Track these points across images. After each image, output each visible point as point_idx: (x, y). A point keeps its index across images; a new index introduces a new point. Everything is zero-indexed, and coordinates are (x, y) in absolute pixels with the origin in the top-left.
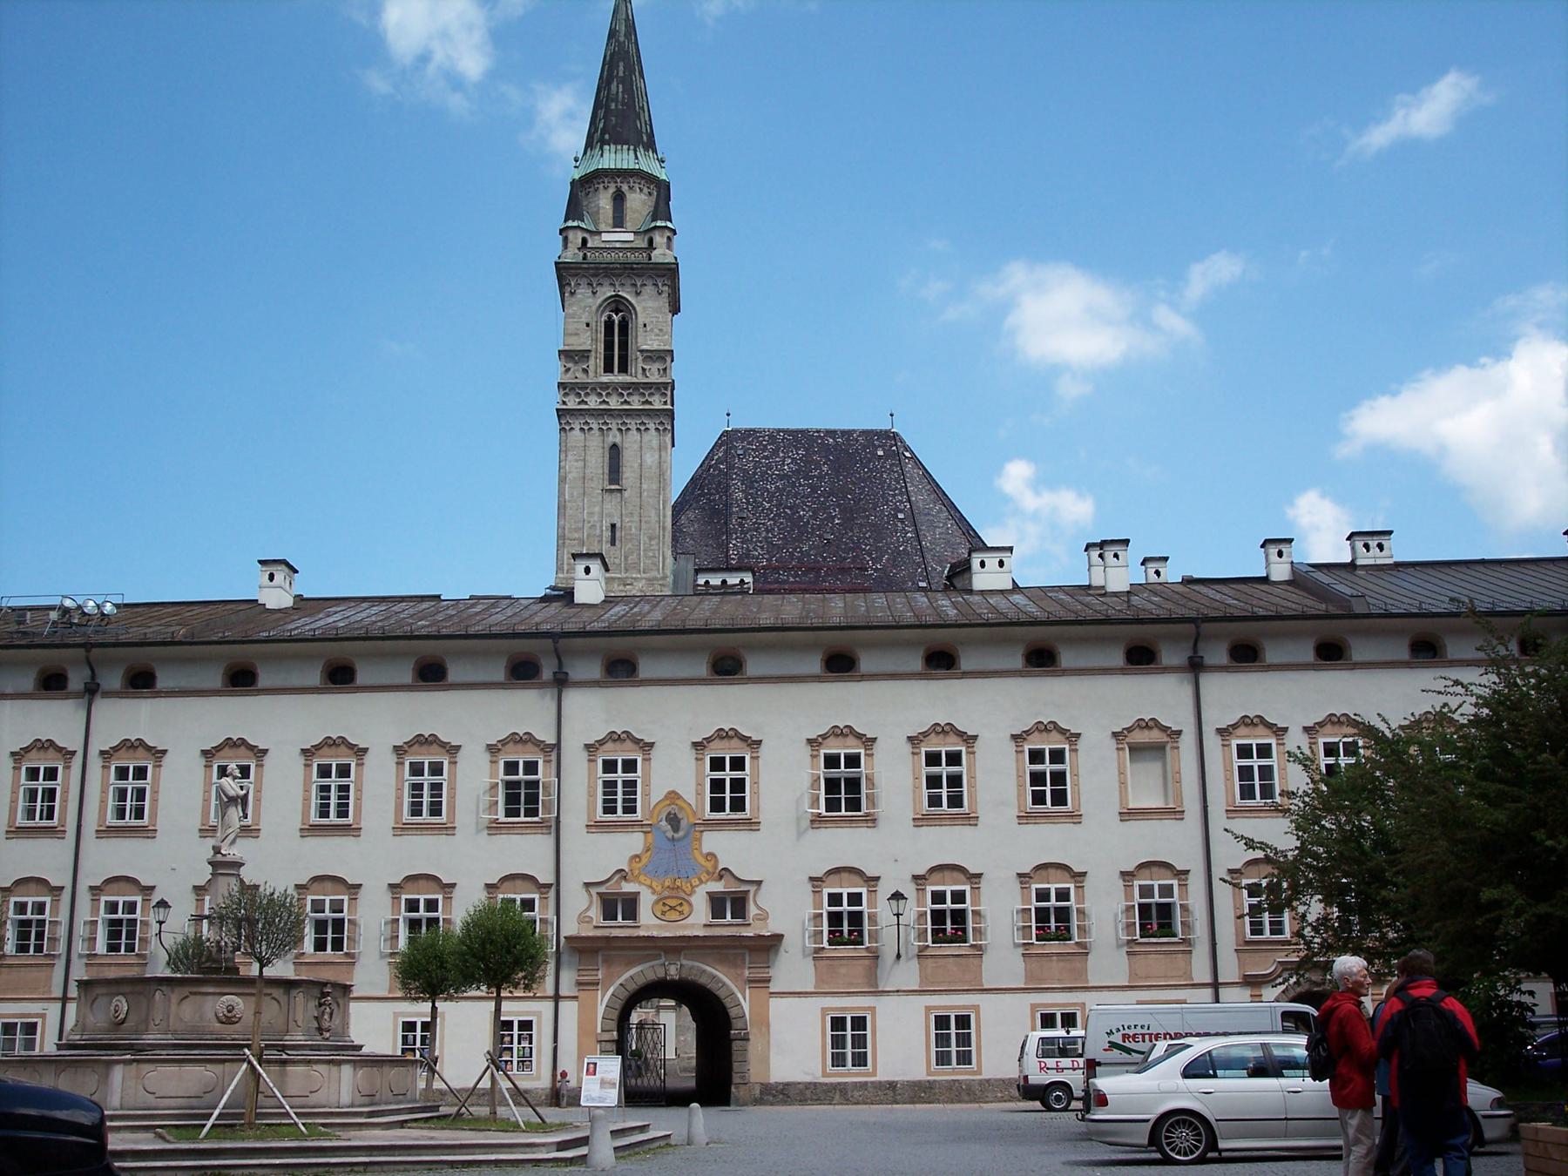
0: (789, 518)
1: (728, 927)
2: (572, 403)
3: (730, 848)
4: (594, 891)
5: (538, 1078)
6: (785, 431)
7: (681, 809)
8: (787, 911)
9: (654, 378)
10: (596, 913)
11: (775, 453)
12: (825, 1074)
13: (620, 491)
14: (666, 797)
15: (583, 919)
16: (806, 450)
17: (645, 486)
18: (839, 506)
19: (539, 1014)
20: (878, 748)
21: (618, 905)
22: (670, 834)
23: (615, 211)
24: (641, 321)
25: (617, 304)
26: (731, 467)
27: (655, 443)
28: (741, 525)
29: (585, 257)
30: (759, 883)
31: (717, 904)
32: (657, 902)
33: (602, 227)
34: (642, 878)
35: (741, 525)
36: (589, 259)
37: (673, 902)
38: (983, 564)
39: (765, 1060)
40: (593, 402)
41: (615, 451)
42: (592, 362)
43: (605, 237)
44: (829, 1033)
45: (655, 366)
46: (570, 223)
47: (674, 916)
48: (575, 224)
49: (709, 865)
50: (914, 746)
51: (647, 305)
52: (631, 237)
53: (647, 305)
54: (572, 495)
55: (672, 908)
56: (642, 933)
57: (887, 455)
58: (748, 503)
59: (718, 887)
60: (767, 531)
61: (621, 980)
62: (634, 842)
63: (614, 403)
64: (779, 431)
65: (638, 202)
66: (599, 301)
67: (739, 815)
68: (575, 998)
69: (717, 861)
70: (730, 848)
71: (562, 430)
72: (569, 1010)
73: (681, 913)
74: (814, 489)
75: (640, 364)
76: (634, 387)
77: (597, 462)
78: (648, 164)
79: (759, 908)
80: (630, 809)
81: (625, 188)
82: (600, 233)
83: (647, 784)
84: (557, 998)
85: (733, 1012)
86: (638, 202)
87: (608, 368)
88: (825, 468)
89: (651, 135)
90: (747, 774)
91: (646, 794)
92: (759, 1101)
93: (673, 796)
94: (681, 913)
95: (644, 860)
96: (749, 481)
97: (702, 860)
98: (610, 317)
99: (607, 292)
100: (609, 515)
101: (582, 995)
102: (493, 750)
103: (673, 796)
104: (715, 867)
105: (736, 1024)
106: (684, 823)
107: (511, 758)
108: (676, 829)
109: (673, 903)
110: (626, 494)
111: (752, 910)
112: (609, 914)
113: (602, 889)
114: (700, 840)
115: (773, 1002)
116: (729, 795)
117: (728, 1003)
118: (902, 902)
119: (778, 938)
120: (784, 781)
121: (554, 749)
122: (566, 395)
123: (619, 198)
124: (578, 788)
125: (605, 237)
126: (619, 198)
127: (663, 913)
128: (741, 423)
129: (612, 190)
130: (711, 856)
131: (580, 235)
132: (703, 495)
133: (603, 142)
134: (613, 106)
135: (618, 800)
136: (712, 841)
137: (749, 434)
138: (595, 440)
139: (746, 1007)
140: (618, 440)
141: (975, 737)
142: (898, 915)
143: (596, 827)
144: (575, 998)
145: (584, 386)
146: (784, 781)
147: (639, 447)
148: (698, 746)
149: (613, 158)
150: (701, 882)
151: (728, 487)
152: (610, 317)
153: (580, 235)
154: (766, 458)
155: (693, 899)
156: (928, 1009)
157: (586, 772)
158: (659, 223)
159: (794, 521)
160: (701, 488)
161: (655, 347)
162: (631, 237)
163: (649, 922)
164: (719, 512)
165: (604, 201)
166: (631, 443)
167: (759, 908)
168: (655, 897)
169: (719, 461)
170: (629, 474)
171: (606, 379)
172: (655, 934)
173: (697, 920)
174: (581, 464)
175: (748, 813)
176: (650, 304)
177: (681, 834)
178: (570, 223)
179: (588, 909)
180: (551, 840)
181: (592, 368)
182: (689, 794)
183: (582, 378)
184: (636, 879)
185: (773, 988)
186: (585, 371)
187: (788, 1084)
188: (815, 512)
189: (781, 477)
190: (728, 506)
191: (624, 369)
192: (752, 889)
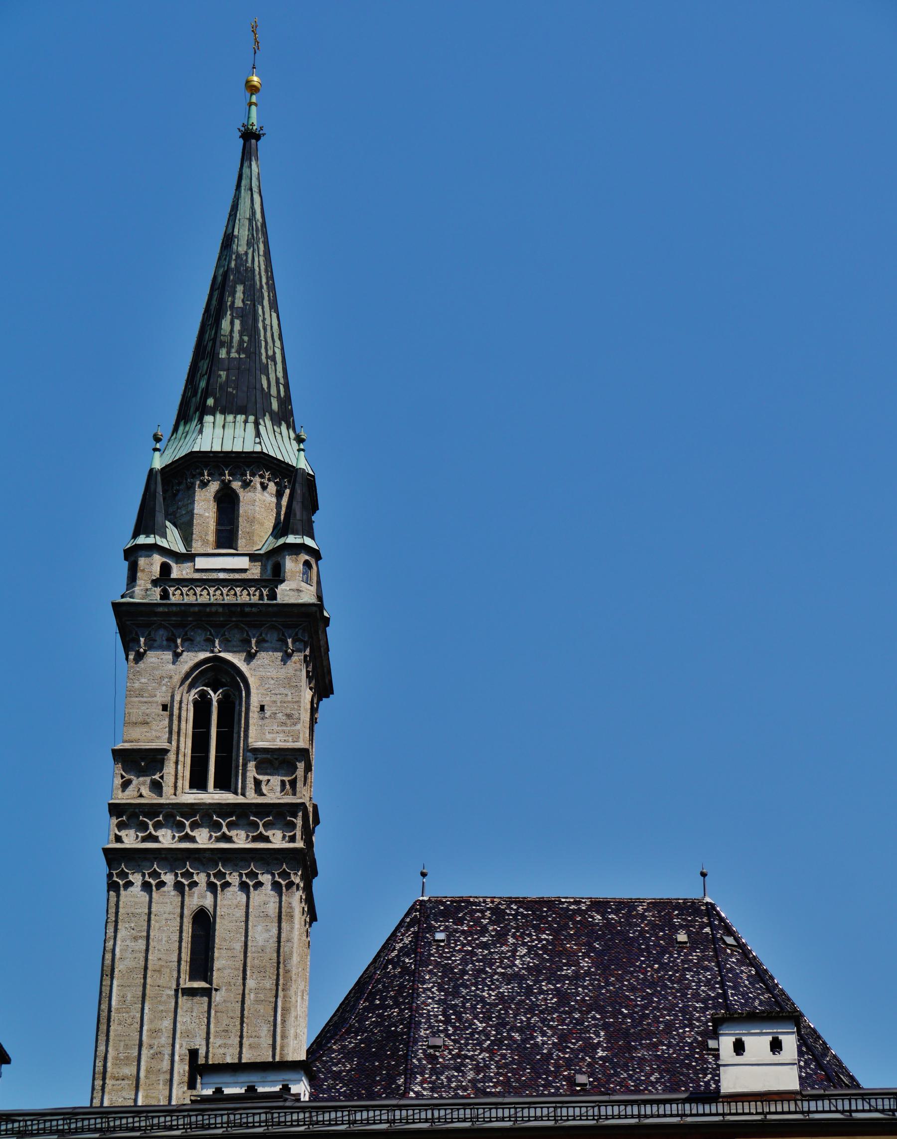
0: (519, 1048)
2: (131, 840)
6: (522, 902)
11: (501, 938)
13: (207, 993)
16: (556, 933)
17: (250, 983)
18: (606, 1026)
23: (220, 521)
24: (255, 701)
26: (423, 962)
27: (272, 908)
28: (432, 1059)
29: (165, 595)
33: (197, 547)
35: (432, 1059)
36: (174, 599)
38: (739, 1048)
40: (167, 839)
41: (204, 923)
42: (169, 769)
43: (201, 563)
46: (142, 540)
48: (150, 540)
51: (271, 680)
52: (243, 562)
53: (271, 680)
54: (123, 999)
57: (696, 940)
58: (447, 1021)
60: (477, 1069)
63: (203, 839)
64: (510, 901)
65: (260, 505)
71: (113, 886)
74: (563, 997)
75: (252, 772)
76: (241, 815)
77: (170, 940)
78: (280, 445)
81: (236, 485)
86: (260, 505)
87: (198, 782)
88: (585, 963)
89: (286, 402)
96: (451, 982)
98: (203, 694)
99: (191, 659)
100: (188, 1034)
110: (217, 997)
122: (120, 826)
123: (227, 504)
125: (201, 563)
126: (227, 504)
128: (447, 886)
129: (214, 486)
132: (372, 1008)
133: (204, 411)
134: (223, 354)
137: (456, 909)
138: (166, 902)
145: (152, 810)
147: (247, 913)
149: (220, 435)
151: (414, 995)
152: (203, 694)
153: (158, 560)
154: (484, 946)
158: (291, 539)
159: (527, 1053)
160: (371, 997)
162: (243, 562)
164: (393, 1037)
165: (204, 506)
166: (230, 903)
170: (224, 962)
174: (142, 944)
178: (142, 540)
181: (169, 781)
183: (150, 798)
186: (157, 787)
188: (564, 1038)
189: (508, 979)
190: (412, 1025)
191: (224, 783)
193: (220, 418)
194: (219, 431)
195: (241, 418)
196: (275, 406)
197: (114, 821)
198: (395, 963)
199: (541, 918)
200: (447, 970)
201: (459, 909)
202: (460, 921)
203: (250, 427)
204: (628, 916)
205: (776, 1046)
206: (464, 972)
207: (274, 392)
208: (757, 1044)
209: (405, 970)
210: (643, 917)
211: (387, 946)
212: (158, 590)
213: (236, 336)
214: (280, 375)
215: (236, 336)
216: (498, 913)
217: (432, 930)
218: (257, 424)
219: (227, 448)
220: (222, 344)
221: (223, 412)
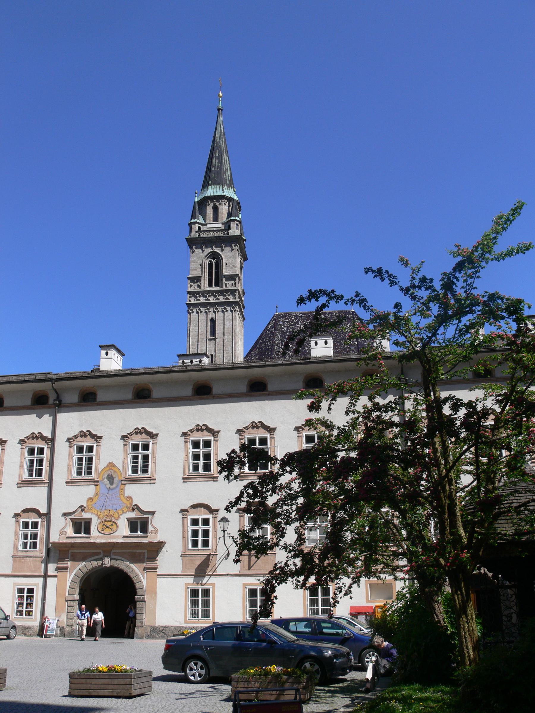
1: (138, 538)
2: (193, 300)
3: (140, 494)
4: (68, 518)
5: (35, 620)
7: (115, 472)
8: (169, 531)
9: (230, 287)
10: (70, 531)
11: (297, 323)
12: (186, 622)
14: (108, 466)
15: (62, 533)
19: (37, 585)
20: (221, 436)
21: (82, 526)
22: (109, 486)
23: (214, 214)
25: (215, 256)
26: (276, 330)
29: (199, 235)
30: (153, 513)
31: (133, 525)
32: (100, 523)
34: (93, 510)
37: (108, 524)
38: (316, 343)
39: (154, 613)
40: (202, 300)
41: (213, 321)
42: (202, 281)
43: (209, 226)
44: (189, 598)
45: (230, 283)
47: (107, 531)
48: (195, 221)
49: (128, 503)
50: (240, 435)
55: (108, 527)
56: (92, 541)
59: (132, 515)
61: (80, 567)
62: (89, 490)
63: (212, 299)
66: (206, 254)
67: (145, 475)
68: (56, 576)
69: (132, 501)
70: (140, 494)
72: (52, 582)
73: (112, 529)
76: (222, 293)
79: (153, 527)
80: (89, 473)
81: (217, 204)
82: (206, 225)
83: (98, 459)
84: (46, 576)
85: (137, 585)
87: (210, 285)
90: (150, 452)
91: (97, 465)
92: (149, 637)
93: (111, 465)
94: (112, 529)
95: (95, 500)
97: (125, 501)
98: (211, 261)
101: (59, 574)
102: (22, 442)
103: (111, 465)
104: (131, 504)
105: (139, 592)
106: (116, 480)
107: (32, 446)
108: (112, 483)
109: (108, 524)
111: (150, 528)
112: (77, 530)
113: (72, 517)
114: (123, 489)
115: (159, 580)
116: (142, 465)
117: (135, 580)
118: (227, 523)
119: (160, 545)
120: (170, 457)
121: (51, 441)
122: (190, 297)
123: (216, 209)
124: (64, 459)
125: (209, 226)
126: (216, 209)
127: (103, 529)
130: (129, 498)
131: (197, 225)
135: (85, 466)
136: (131, 490)
137: (285, 316)
138: (203, 316)
139: (144, 582)
140: (214, 316)
141: (274, 429)
142: (224, 531)
143: (71, 482)
144: (56, 576)
146: (170, 457)
148: (124, 438)
150: (123, 512)
151: (274, 338)
152: (211, 261)
154: (293, 325)
155: (118, 522)
156: (15, 584)
157: (68, 453)
158: (232, 218)
161: (231, 273)
162: (220, 225)
163: (96, 536)
166: (219, 317)
167: (153, 527)
168: (99, 521)
169: (272, 327)
170: (219, 332)
171: (208, 289)
172: (98, 541)
173: (122, 533)
175: (150, 474)
176: (228, 254)
177: (114, 486)
178: (193, 221)
179: (64, 528)
180: (45, 490)
182: (119, 464)
184: (90, 511)
185: (159, 572)
186: (199, 286)
187: (165, 627)
190: (273, 346)
191: (217, 284)
192: (150, 517)
193: (213, 186)
194: (213, 190)
195: (218, 186)
196: (228, 182)
197: (188, 296)
198: (269, 331)
199: (308, 317)
200: (283, 332)
201: (286, 316)
202: (286, 319)
203: (221, 188)
204: (331, 315)
205: (326, 343)
206: (287, 332)
207: (227, 178)
208: (321, 342)
209: (272, 332)
210: (335, 315)
211: (267, 326)
212: (197, 234)
213: (217, 164)
214: (229, 174)
215: (217, 164)
216: (297, 316)
217: (279, 321)
218: (223, 188)
219: (215, 195)
220: (213, 167)
221: (214, 185)
